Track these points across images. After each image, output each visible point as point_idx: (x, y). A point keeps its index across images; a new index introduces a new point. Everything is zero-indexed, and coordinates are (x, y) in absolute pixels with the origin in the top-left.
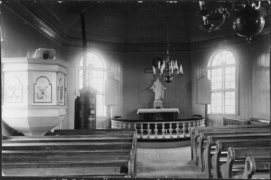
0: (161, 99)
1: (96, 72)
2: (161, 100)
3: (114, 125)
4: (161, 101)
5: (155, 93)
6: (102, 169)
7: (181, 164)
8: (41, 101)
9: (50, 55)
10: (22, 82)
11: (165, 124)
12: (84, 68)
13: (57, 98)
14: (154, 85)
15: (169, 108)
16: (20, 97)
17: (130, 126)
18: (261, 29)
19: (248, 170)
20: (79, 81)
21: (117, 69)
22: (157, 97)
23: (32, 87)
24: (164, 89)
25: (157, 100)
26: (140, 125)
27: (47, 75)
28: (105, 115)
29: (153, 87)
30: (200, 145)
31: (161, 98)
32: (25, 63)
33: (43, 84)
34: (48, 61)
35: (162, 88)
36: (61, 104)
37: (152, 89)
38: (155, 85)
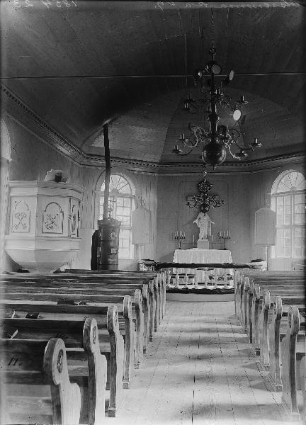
1: (125, 204)
3: (143, 268)
6: (299, 381)
7: (222, 318)
8: (49, 231)
9: (63, 178)
10: (30, 209)
12: (106, 194)
13: (69, 229)
16: (28, 226)
20: (13, 148)
21: (150, 198)
23: (41, 217)
27: (57, 200)
28: (131, 257)
29: (196, 221)
30: (287, 339)
32: (35, 186)
33: (54, 210)
34: (61, 184)
36: (73, 236)
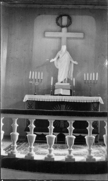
0: (69, 81)
2: (68, 82)
4: (69, 84)
5: (58, 69)
11: (76, 121)
14: (57, 57)
15: (90, 96)
17: (34, 127)
18: (2, 128)
19: (74, 154)
22: (62, 77)
24: (74, 64)
25: (62, 82)
26: (29, 123)
31: (68, 79)
35: (71, 62)
37: (54, 62)
38: (59, 58)
